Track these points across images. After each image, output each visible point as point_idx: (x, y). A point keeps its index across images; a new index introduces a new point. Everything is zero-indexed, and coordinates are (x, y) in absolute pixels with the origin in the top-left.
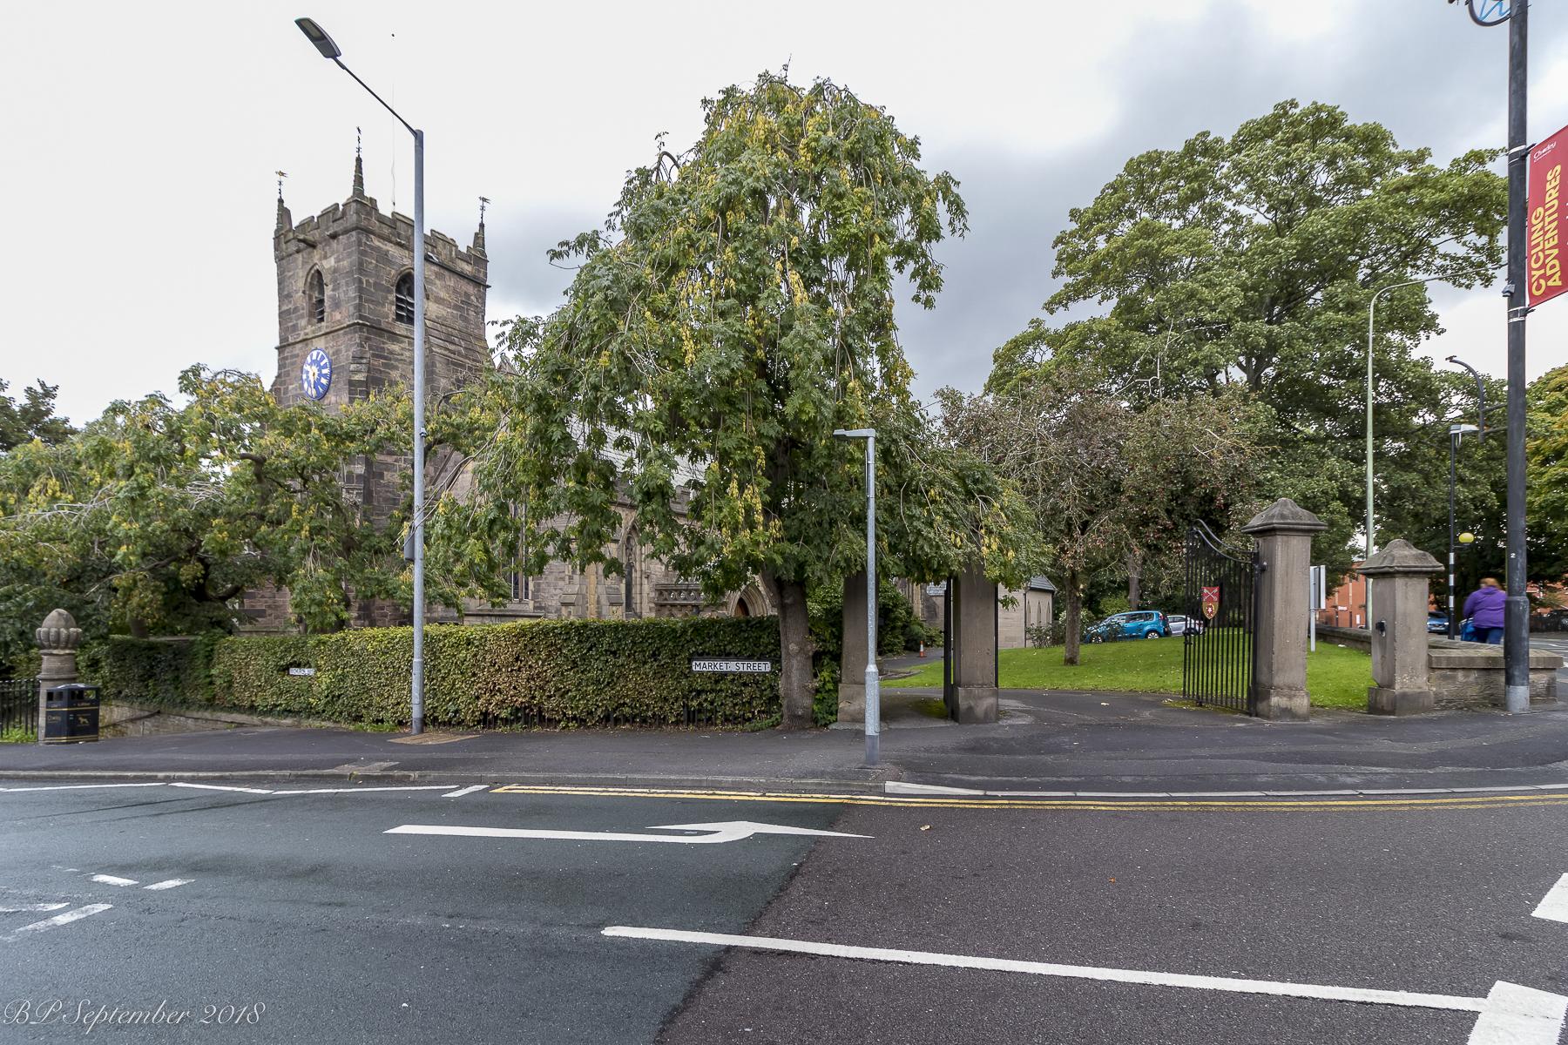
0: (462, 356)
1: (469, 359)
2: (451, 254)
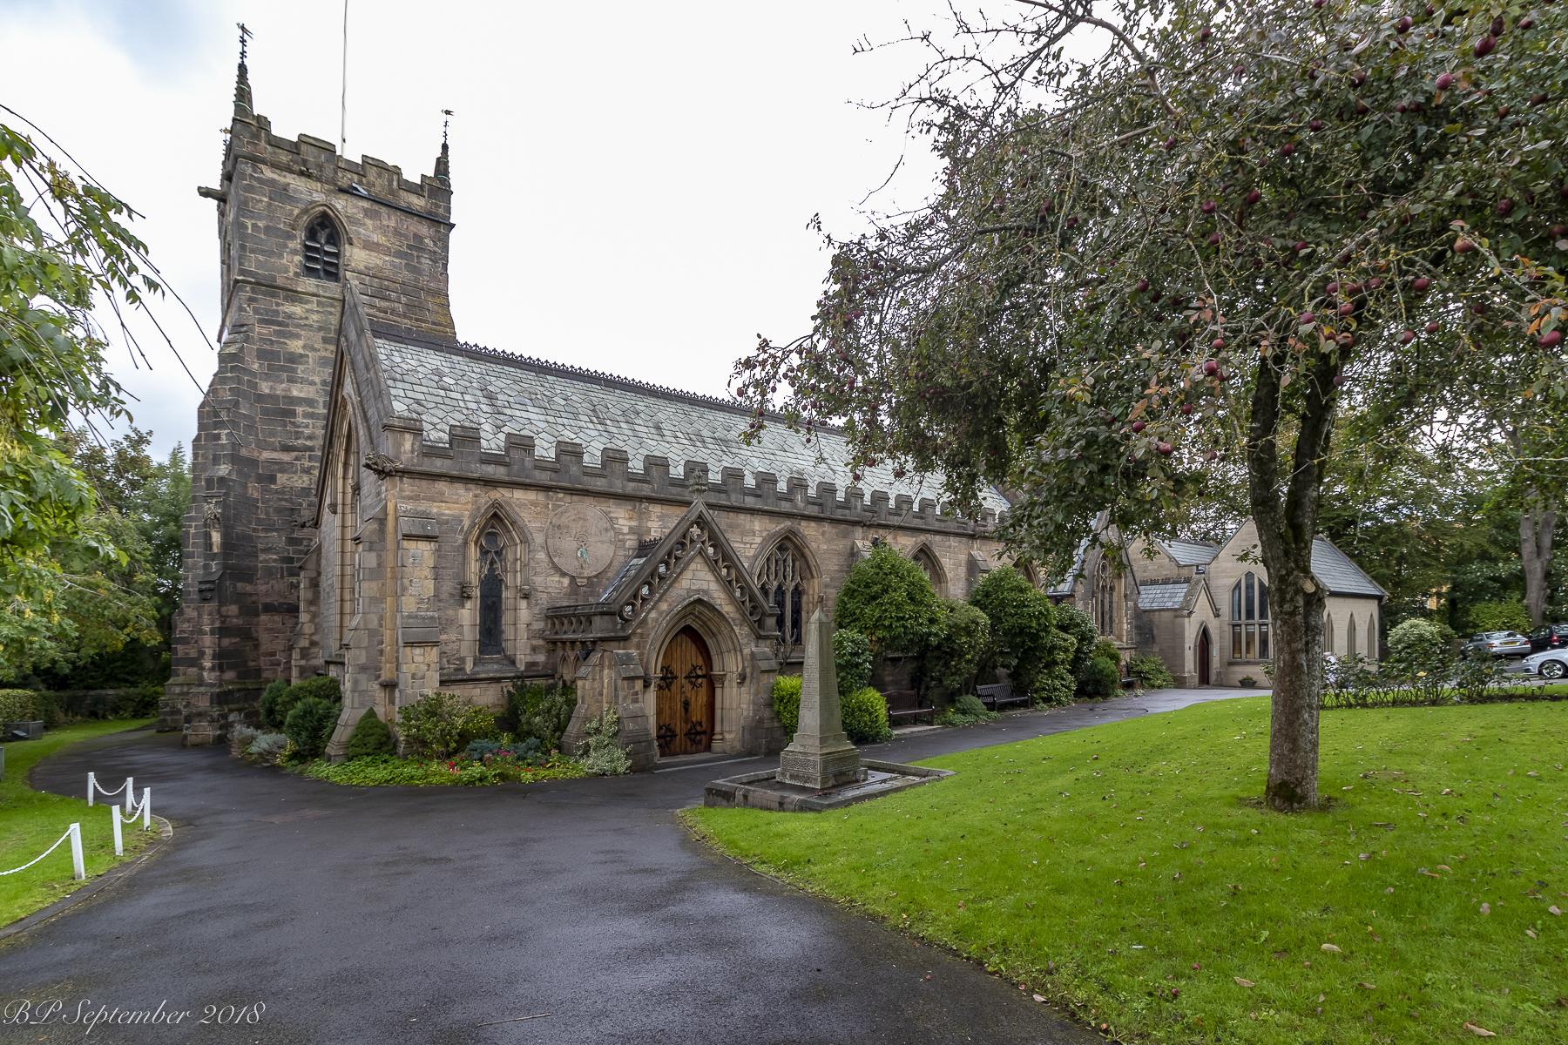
0: (399, 315)
1: (411, 319)
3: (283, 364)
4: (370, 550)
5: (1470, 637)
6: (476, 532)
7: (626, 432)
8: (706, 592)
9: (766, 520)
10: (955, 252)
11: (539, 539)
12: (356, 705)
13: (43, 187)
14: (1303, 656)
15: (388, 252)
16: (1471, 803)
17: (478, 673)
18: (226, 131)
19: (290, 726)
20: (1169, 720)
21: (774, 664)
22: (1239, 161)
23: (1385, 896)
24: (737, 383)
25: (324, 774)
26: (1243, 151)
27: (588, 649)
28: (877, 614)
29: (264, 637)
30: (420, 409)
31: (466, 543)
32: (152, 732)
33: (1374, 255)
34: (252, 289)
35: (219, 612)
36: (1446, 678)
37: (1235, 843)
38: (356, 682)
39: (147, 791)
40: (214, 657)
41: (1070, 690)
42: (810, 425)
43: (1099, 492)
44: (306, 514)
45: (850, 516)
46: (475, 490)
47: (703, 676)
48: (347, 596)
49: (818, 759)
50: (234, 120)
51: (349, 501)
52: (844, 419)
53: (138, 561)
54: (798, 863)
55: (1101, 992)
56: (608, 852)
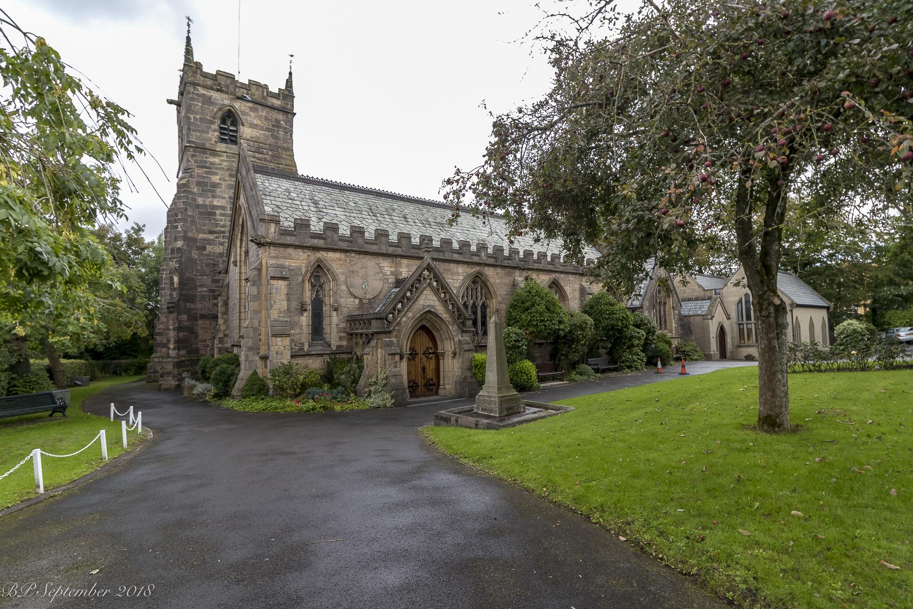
0: (268, 161)
1: (274, 163)
2: (263, 94)
3: (209, 188)
4: (254, 285)
5: (886, 331)
6: (309, 275)
7: (388, 220)
8: (433, 307)
9: (465, 266)
10: (561, 119)
11: (342, 278)
12: (247, 368)
13: (86, 103)
14: (776, 342)
15: (262, 129)
16: (884, 429)
17: (311, 351)
18: (180, 70)
19: (214, 380)
20: (701, 379)
21: (472, 346)
22: (718, 63)
23: (831, 483)
24: (443, 192)
25: (231, 406)
26: (719, 58)
27: (369, 338)
28: (529, 319)
29: (200, 332)
30: (279, 210)
31: (303, 281)
32: (144, 382)
33: (799, 113)
34: (194, 150)
35: (177, 318)
36: (870, 355)
37: (740, 450)
38: (247, 356)
39: (140, 413)
40: (175, 342)
41: (643, 361)
42: (484, 214)
43: (646, 248)
44: (222, 267)
45: (511, 263)
46: (308, 253)
47: (433, 353)
48: (243, 310)
49: (497, 400)
50: (184, 65)
51: (243, 259)
52: (504, 211)
53: (137, 292)
54: (485, 458)
55: (658, 536)
56: (380, 450)
